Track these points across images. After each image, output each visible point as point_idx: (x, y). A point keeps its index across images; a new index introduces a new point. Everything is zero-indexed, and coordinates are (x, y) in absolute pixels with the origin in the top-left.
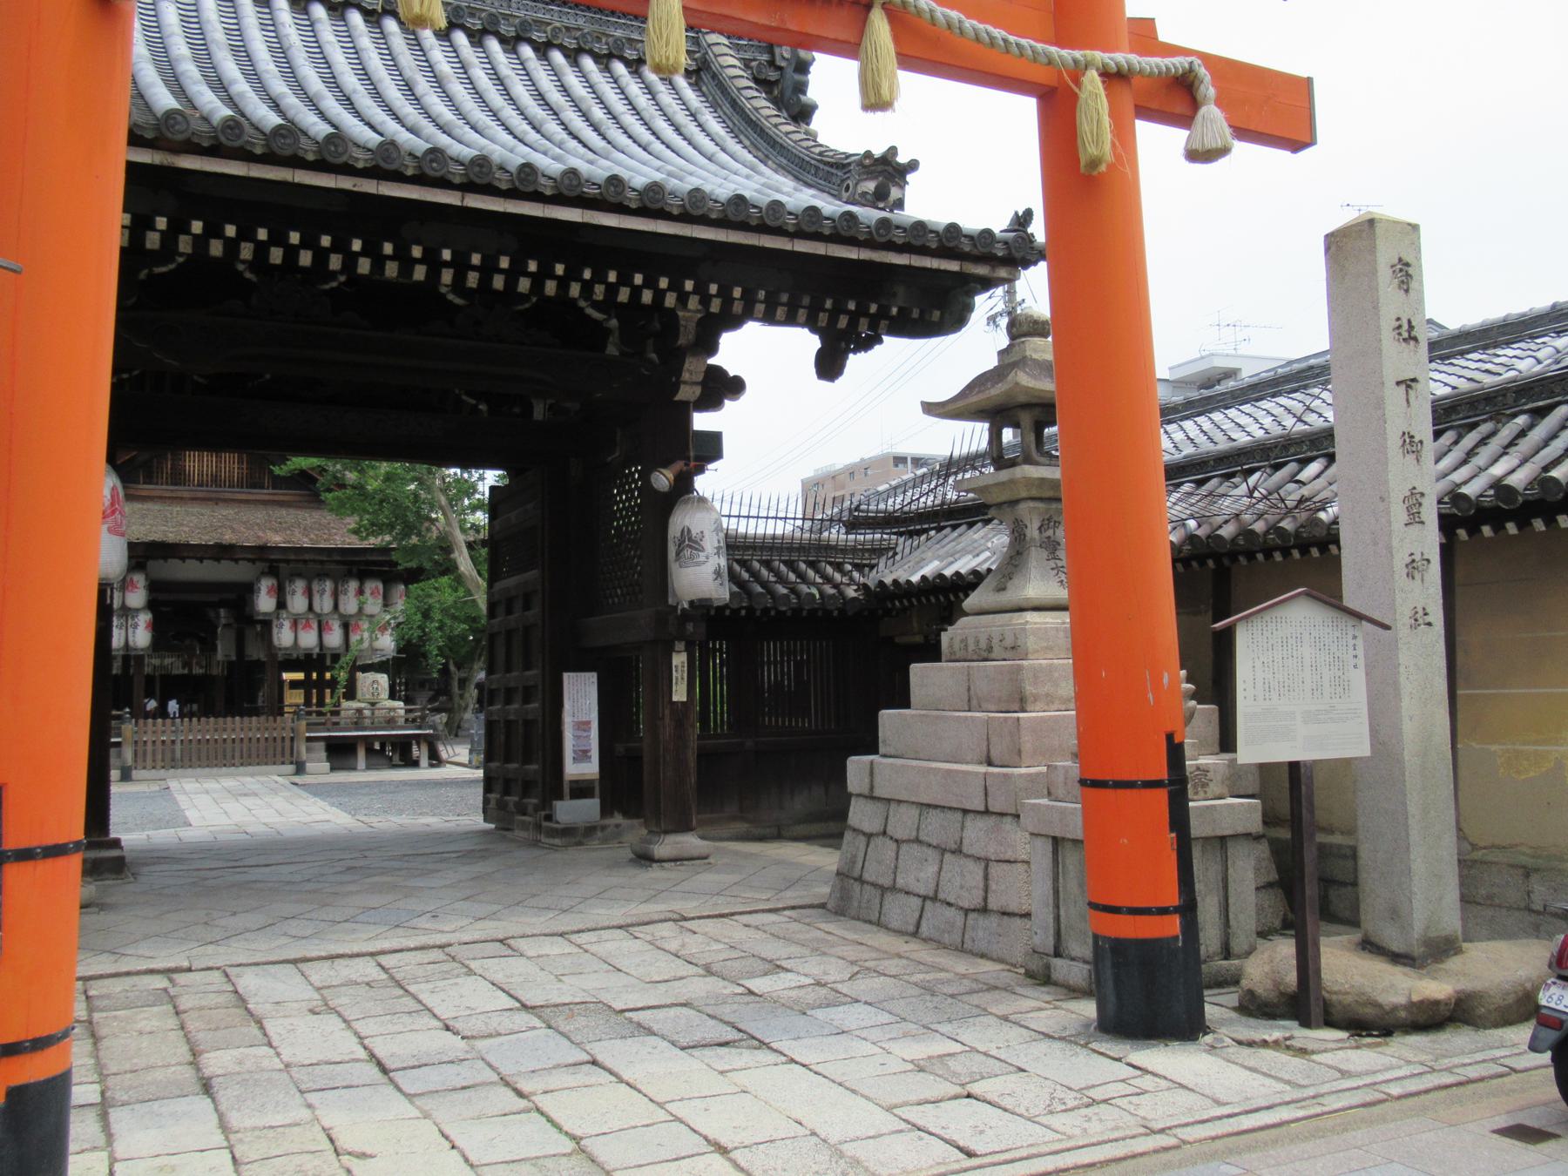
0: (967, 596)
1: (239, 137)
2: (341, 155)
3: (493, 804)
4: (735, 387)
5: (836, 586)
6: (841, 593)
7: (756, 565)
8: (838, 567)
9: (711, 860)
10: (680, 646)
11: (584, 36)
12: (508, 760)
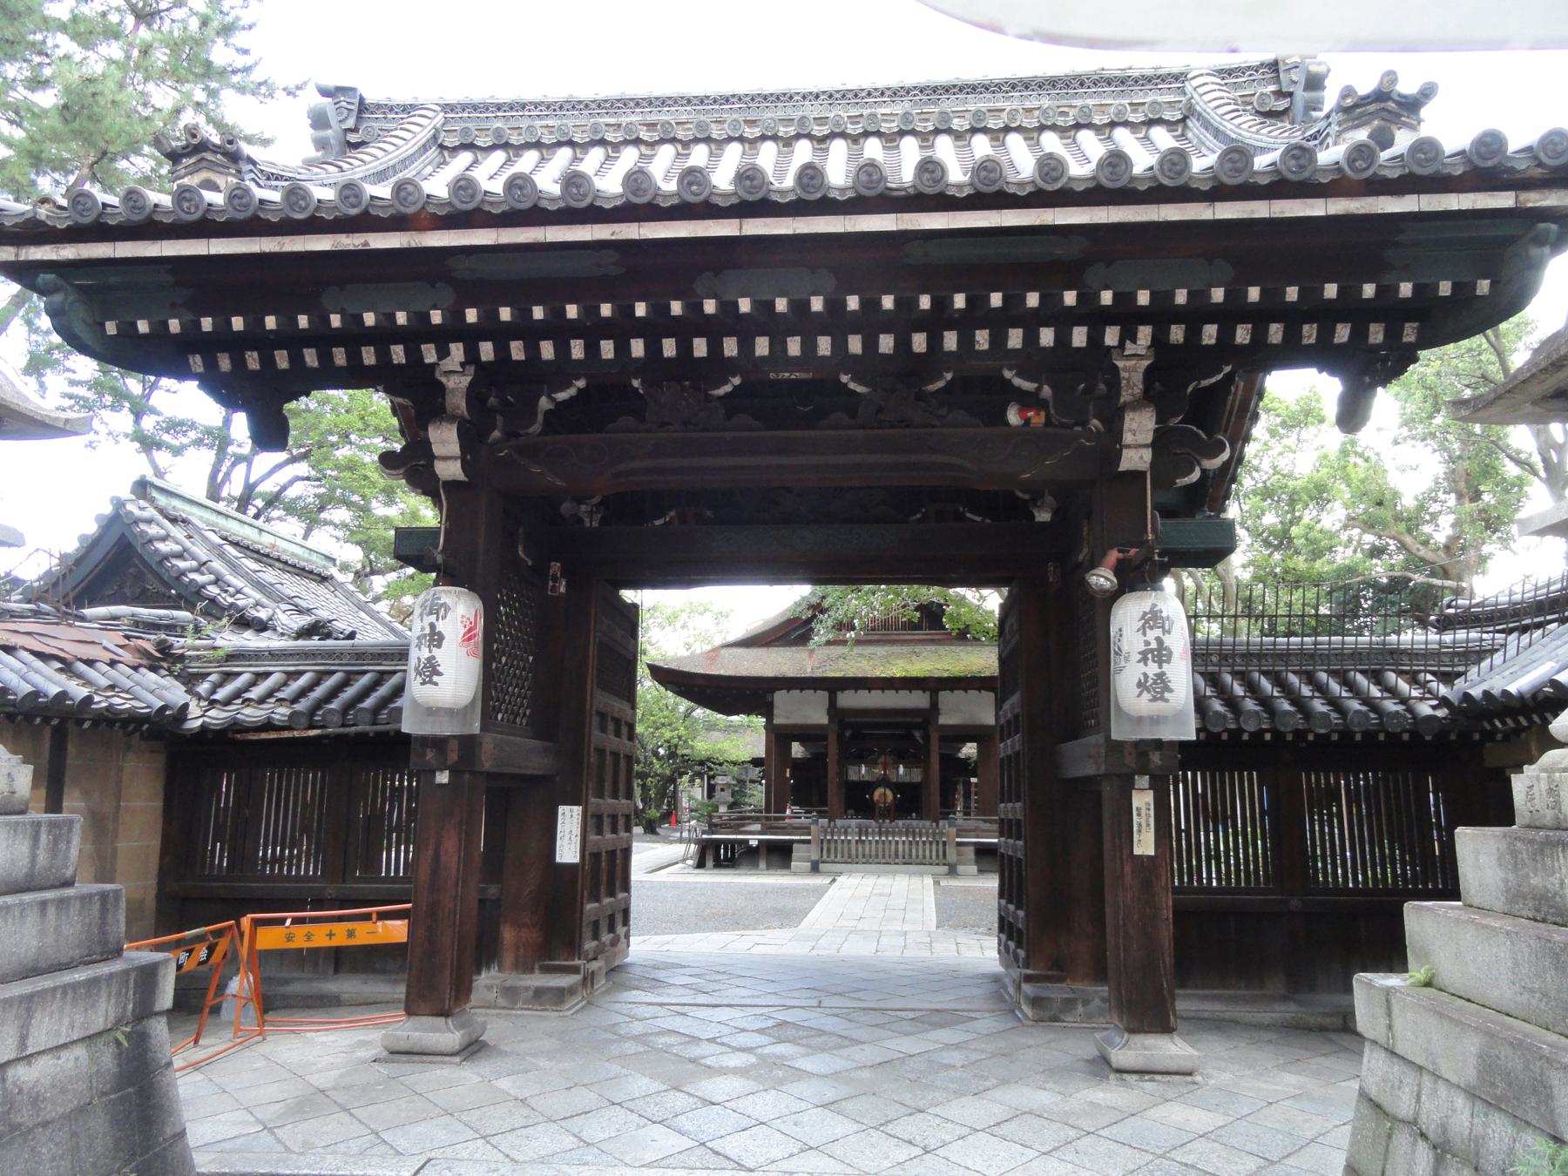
0: (1556, 716)
1: (473, 196)
2: (585, 196)
5: (1404, 701)
6: (1410, 710)
7: (1323, 676)
8: (1413, 679)
9: (1198, 1078)
10: (1143, 781)
11: (1045, 112)
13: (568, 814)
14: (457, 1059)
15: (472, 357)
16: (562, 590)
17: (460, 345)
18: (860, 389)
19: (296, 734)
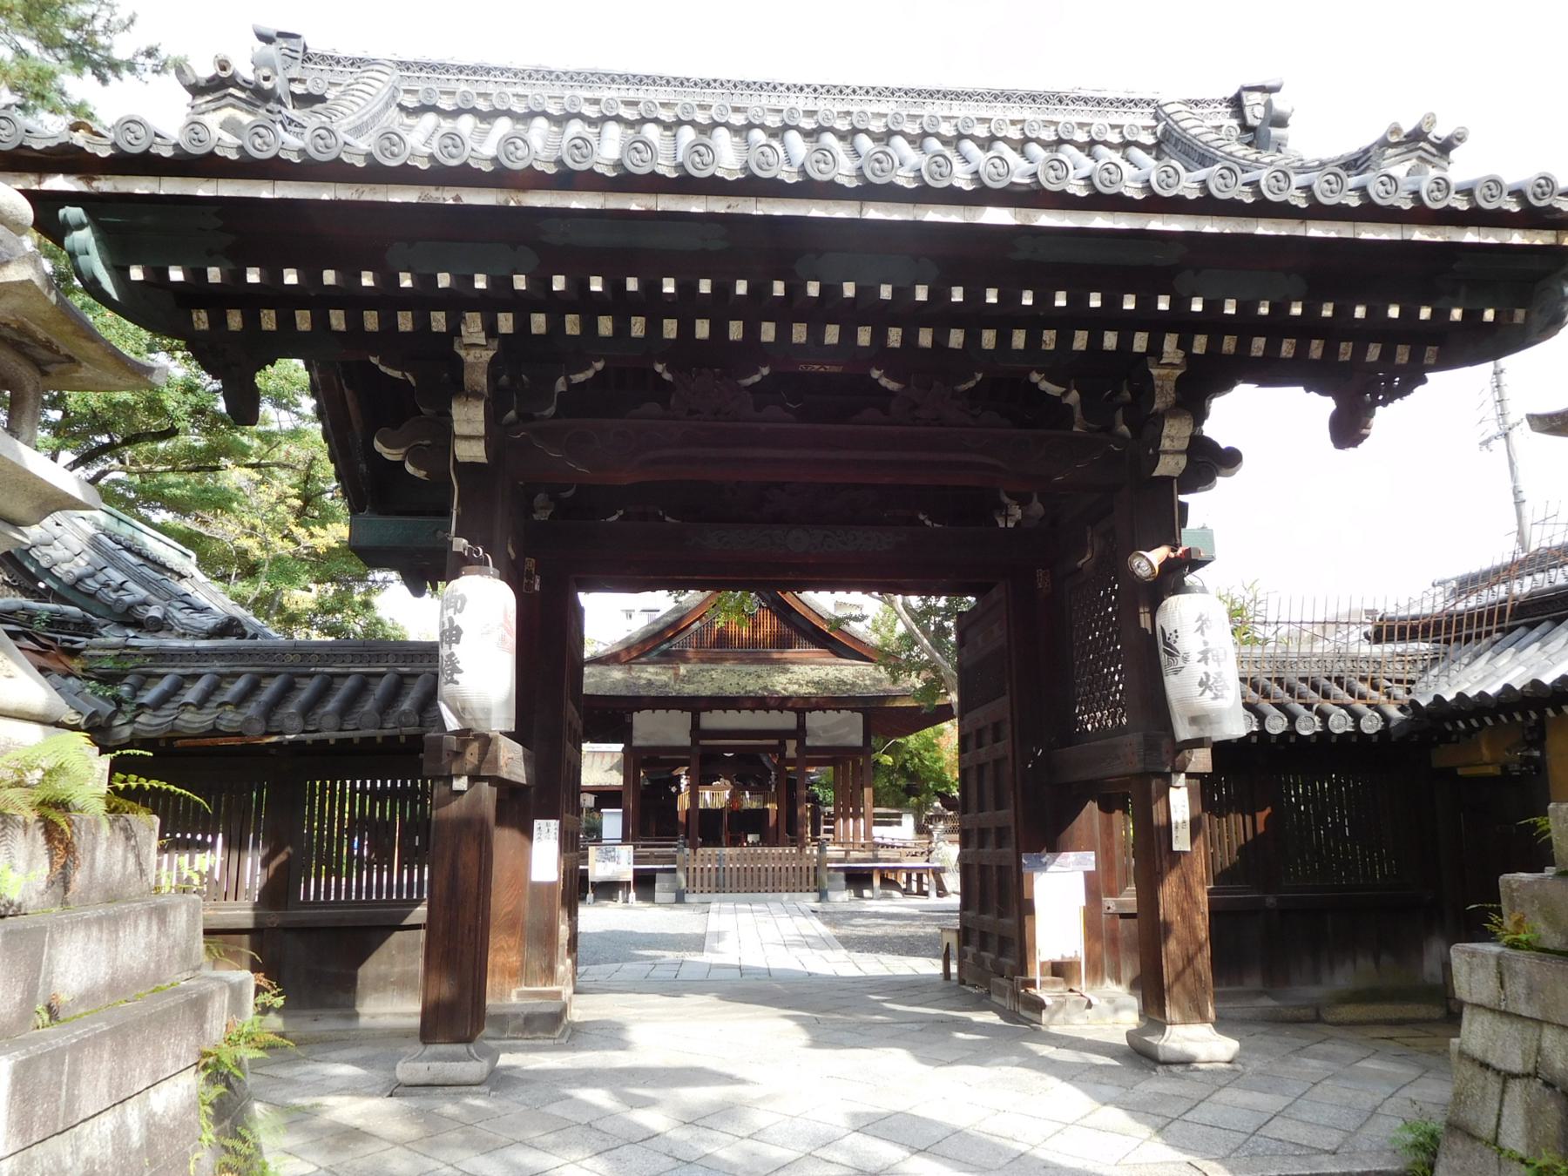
3: (969, 960)
4: (1230, 459)
12: (983, 911)
13: (544, 829)
14: (485, 1089)
15: (491, 329)
16: (537, 587)
17: (510, 316)
18: (892, 386)
19: (131, 752)
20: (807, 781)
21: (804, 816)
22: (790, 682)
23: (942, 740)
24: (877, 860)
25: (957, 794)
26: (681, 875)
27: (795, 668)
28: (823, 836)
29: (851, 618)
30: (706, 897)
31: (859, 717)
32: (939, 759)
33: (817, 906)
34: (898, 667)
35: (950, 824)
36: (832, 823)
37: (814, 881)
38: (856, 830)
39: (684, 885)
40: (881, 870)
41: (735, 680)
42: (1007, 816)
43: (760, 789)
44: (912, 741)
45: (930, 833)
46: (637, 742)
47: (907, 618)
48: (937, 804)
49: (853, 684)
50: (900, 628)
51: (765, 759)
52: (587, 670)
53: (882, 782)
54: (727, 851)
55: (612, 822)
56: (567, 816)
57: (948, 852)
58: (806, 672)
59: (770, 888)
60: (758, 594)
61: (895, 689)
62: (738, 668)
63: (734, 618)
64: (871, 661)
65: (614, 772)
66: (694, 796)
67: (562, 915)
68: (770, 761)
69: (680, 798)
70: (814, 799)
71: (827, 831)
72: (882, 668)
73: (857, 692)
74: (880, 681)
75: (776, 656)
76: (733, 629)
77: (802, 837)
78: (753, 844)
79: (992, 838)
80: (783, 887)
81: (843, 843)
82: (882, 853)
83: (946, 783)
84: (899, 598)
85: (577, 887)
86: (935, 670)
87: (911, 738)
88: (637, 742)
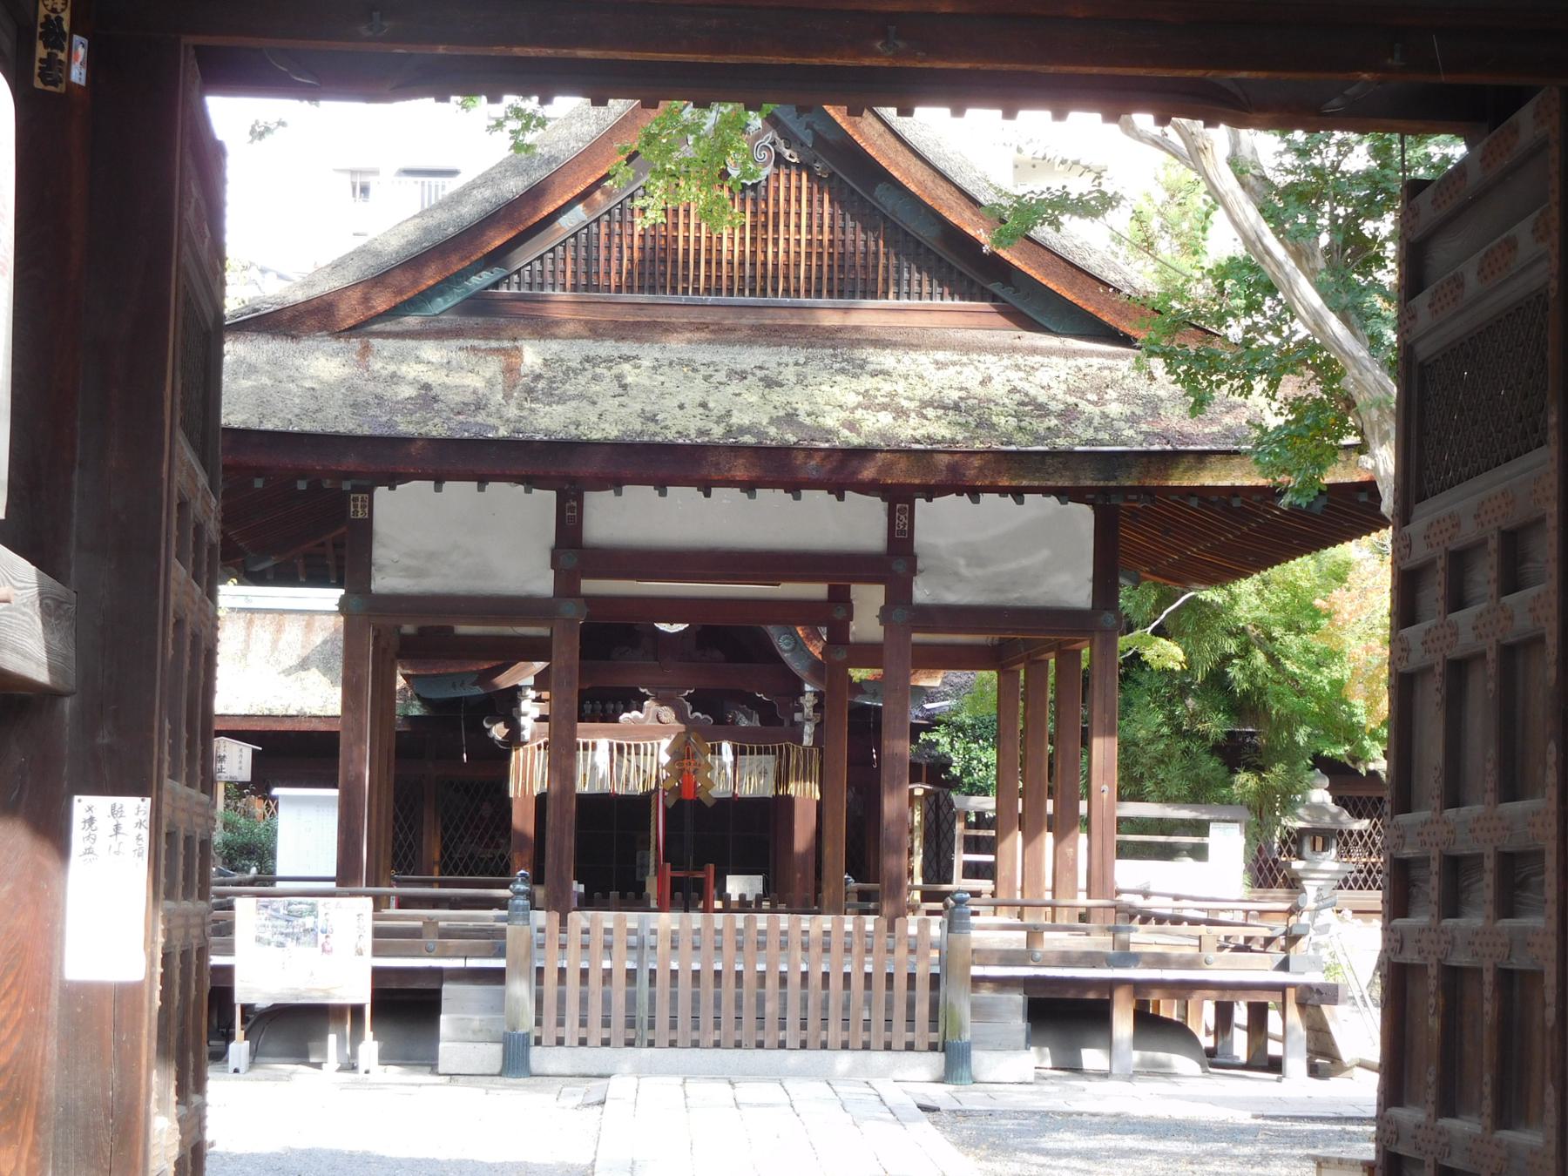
12: (1448, 1105)
13: (104, 823)
16: (78, 74)
20: (914, 715)
21: (902, 818)
22: (869, 402)
23: (1342, 600)
24: (1126, 957)
25: (1380, 765)
26: (519, 989)
27: (885, 359)
28: (959, 883)
29: (1063, 204)
30: (594, 1057)
31: (1083, 517)
32: (1330, 656)
33: (940, 1094)
34: (1208, 362)
35: (1359, 858)
36: (989, 846)
37: (929, 1020)
38: (1063, 868)
39: (527, 1023)
40: (1138, 987)
41: (694, 392)
42: (1534, 817)
43: (770, 733)
44: (1248, 598)
45: (1293, 883)
46: (384, 582)
47: (1250, 214)
48: (1320, 795)
49: (1069, 414)
50: (1223, 244)
51: (783, 644)
52: (234, 350)
53: (1149, 722)
54: (667, 921)
55: (306, 828)
56: (176, 788)
57: (1348, 943)
58: (927, 371)
59: (792, 1034)
60: (772, 121)
61: (1203, 432)
62: (703, 355)
63: (694, 195)
64: (1126, 341)
65: (314, 676)
66: (562, 752)
67: (160, 1084)
68: (798, 649)
69: (518, 757)
70: (934, 771)
71: (972, 871)
72: (1158, 365)
73: (1078, 438)
74: (1153, 406)
75: (831, 319)
76: (690, 234)
77: (896, 887)
78: (744, 905)
79: (1485, 887)
80: (835, 1033)
81: (1036, 901)
82: (1143, 938)
83: (1350, 732)
84: (1219, 138)
85: (203, 1016)
86: (1328, 372)
87: (1245, 587)
88: (384, 582)
